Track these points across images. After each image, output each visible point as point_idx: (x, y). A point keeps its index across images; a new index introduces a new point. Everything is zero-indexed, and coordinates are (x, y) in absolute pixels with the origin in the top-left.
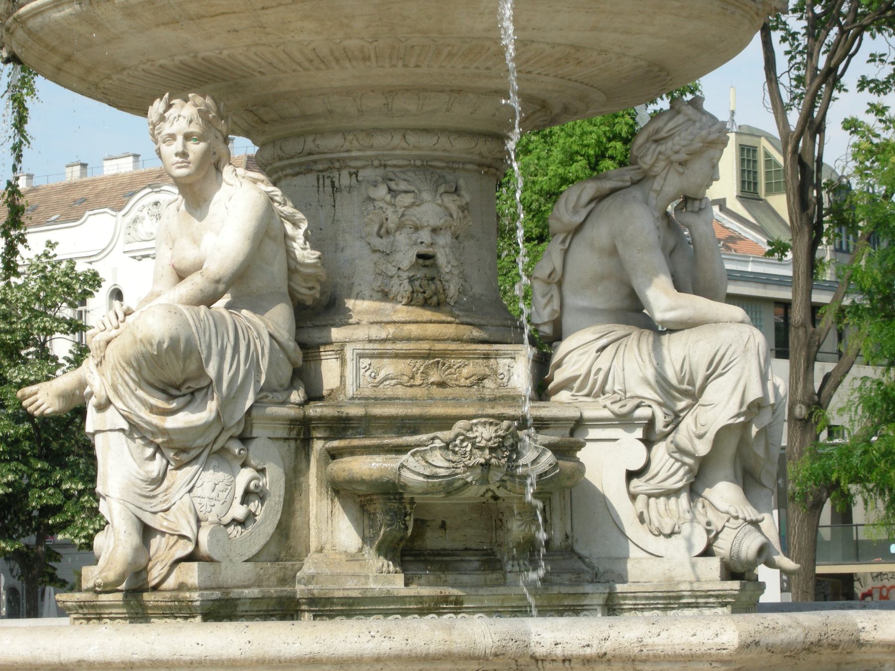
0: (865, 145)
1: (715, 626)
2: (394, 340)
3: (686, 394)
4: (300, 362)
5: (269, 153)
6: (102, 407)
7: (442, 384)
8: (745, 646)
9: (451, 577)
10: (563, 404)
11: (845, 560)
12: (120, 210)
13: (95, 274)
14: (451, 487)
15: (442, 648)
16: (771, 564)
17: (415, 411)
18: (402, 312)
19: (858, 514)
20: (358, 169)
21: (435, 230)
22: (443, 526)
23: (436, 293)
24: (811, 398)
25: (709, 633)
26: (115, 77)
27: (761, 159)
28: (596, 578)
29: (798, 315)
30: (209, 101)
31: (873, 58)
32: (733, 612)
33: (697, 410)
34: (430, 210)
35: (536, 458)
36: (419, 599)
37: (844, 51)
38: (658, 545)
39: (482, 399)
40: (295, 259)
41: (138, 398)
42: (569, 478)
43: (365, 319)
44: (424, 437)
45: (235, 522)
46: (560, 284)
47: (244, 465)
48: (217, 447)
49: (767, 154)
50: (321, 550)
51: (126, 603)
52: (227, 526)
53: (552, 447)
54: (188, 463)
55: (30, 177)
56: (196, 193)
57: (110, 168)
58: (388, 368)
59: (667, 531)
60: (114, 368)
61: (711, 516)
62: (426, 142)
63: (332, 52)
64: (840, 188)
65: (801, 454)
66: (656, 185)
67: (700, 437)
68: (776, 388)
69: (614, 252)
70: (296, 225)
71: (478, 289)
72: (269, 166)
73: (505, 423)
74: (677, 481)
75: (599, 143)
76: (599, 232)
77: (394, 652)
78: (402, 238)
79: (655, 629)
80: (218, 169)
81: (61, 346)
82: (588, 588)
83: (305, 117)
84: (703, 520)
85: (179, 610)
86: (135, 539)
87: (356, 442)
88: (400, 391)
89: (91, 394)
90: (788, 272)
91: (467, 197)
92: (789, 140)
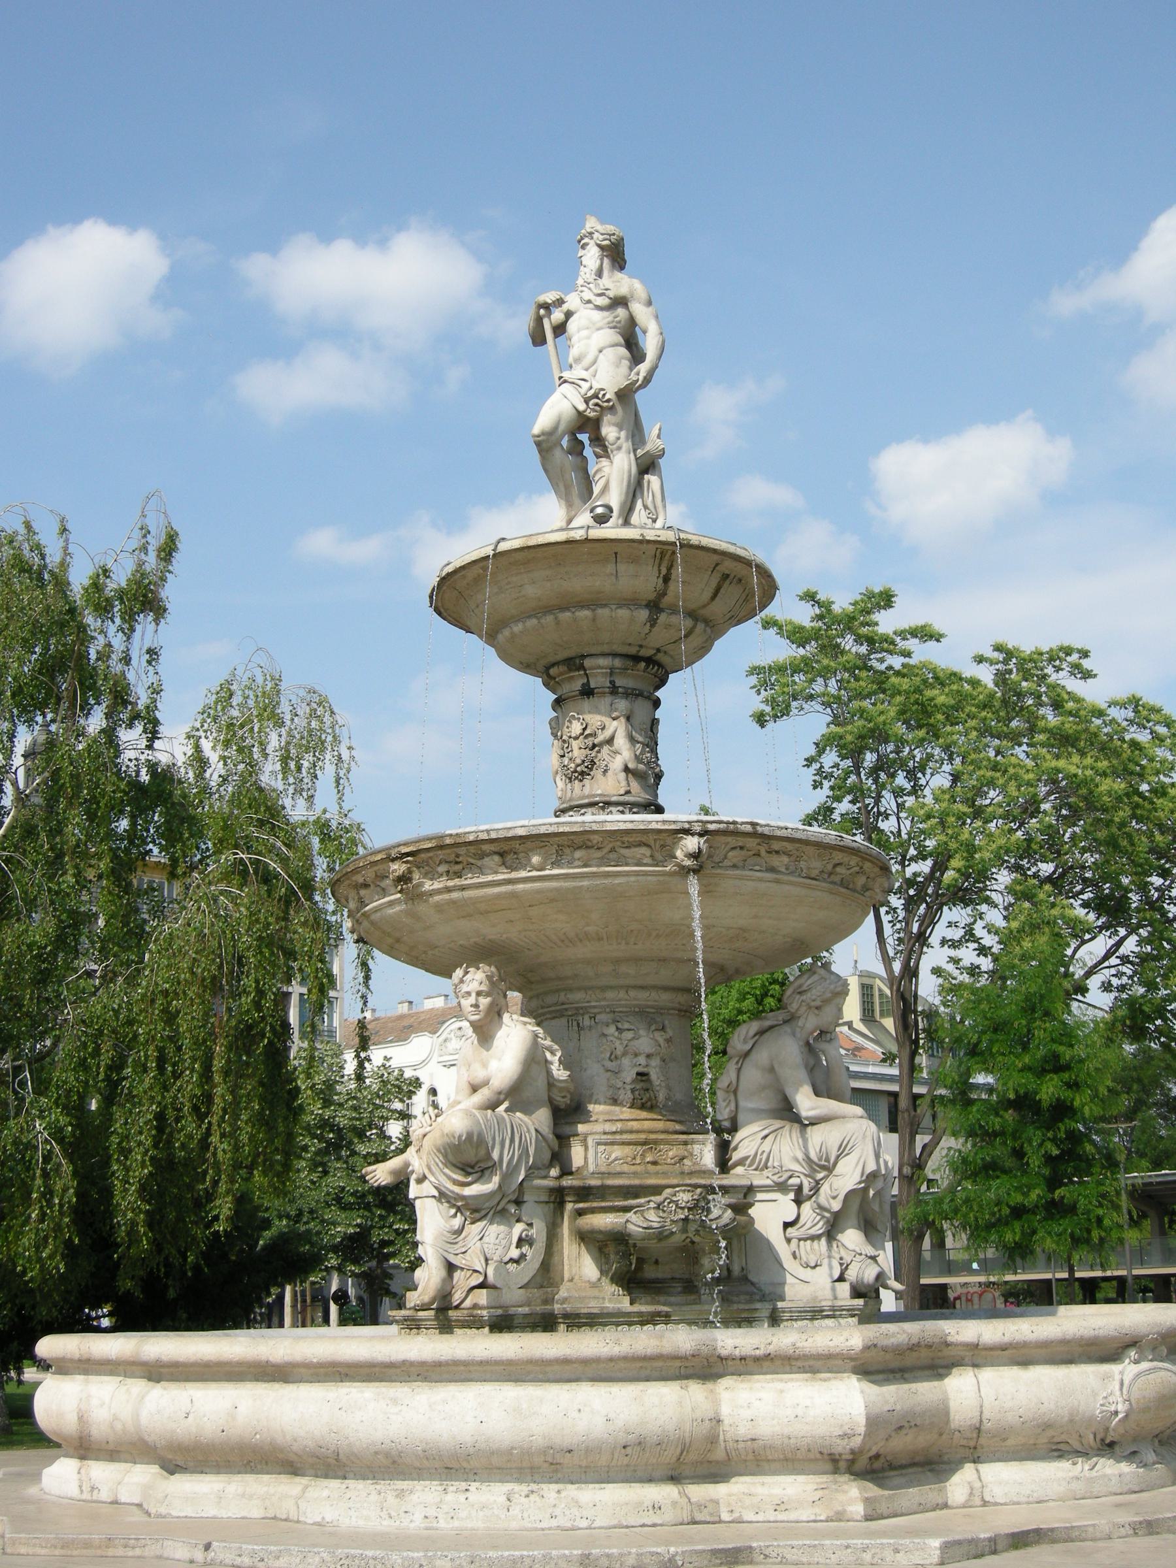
0: (947, 985)
1: (846, 1334)
2: (622, 1132)
3: (823, 1168)
4: (556, 1148)
5: (534, 1003)
6: (421, 1180)
7: (655, 1163)
8: (867, 1348)
9: (662, 1299)
10: (739, 1176)
11: (941, 1274)
12: (435, 1033)
13: (418, 1079)
14: (661, 1235)
15: (656, 1351)
16: (886, 1287)
17: (636, 1182)
18: (626, 1113)
19: (949, 1242)
20: (596, 1014)
21: (648, 1056)
22: (657, 1262)
23: (650, 1099)
24: (914, 1161)
25: (842, 1339)
26: (430, 952)
27: (877, 994)
28: (763, 1298)
29: (903, 1103)
30: (493, 969)
31: (950, 924)
32: (860, 1322)
33: (831, 1179)
34: (645, 1042)
35: (720, 1213)
36: (640, 1314)
37: (930, 920)
38: (806, 1274)
39: (682, 1173)
40: (553, 1076)
41: (445, 1174)
42: (744, 1228)
43: (601, 1118)
44: (642, 1200)
45: (512, 1260)
46: (735, 1092)
47: (518, 1221)
48: (499, 1208)
49: (880, 990)
50: (571, 1280)
51: (437, 1318)
52: (506, 1263)
53: (730, 1206)
54: (479, 1220)
55: (374, 1010)
56: (484, 1032)
57: (429, 1004)
58: (617, 1152)
59: (813, 1264)
60: (429, 1153)
61: (843, 1253)
62: (642, 995)
63: (577, 935)
64: (931, 1014)
65: (908, 1202)
66: (800, 1024)
67: (834, 1198)
68: (886, 1163)
69: (772, 1070)
70: (553, 1053)
71: (679, 1096)
72: (536, 1011)
73: (699, 1190)
74: (819, 1229)
75: (763, 986)
76: (762, 1056)
77: (622, 1354)
78: (626, 1061)
79: (804, 1337)
80: (500, 1015)
81: (394, 1129)
82: (758, 1305)
83: (559, 979)
84: (838, 1256)
85: (473, 1323)
86: (443, 1273)
87: (595, 1204)
88: (626, 1168)
89: (413, 1172)
90: (895, 1071)
91: (670, 1033)
92: (891, 980)
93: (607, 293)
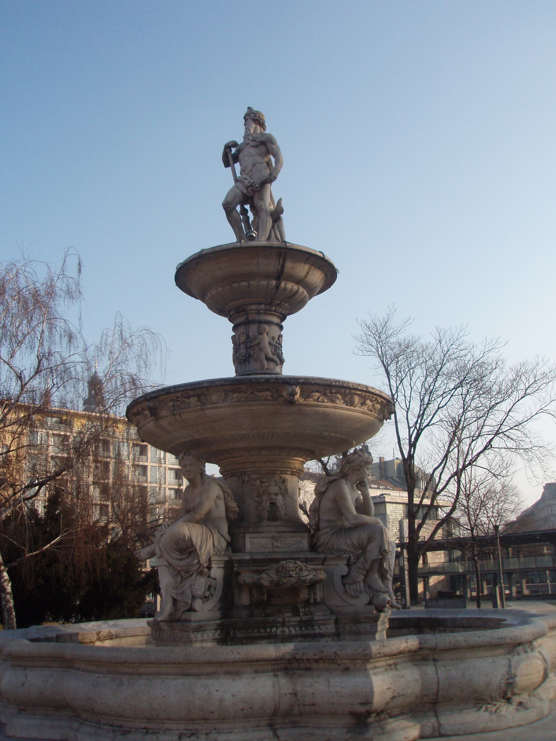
48: (199, 570)
93: (257, 140)
